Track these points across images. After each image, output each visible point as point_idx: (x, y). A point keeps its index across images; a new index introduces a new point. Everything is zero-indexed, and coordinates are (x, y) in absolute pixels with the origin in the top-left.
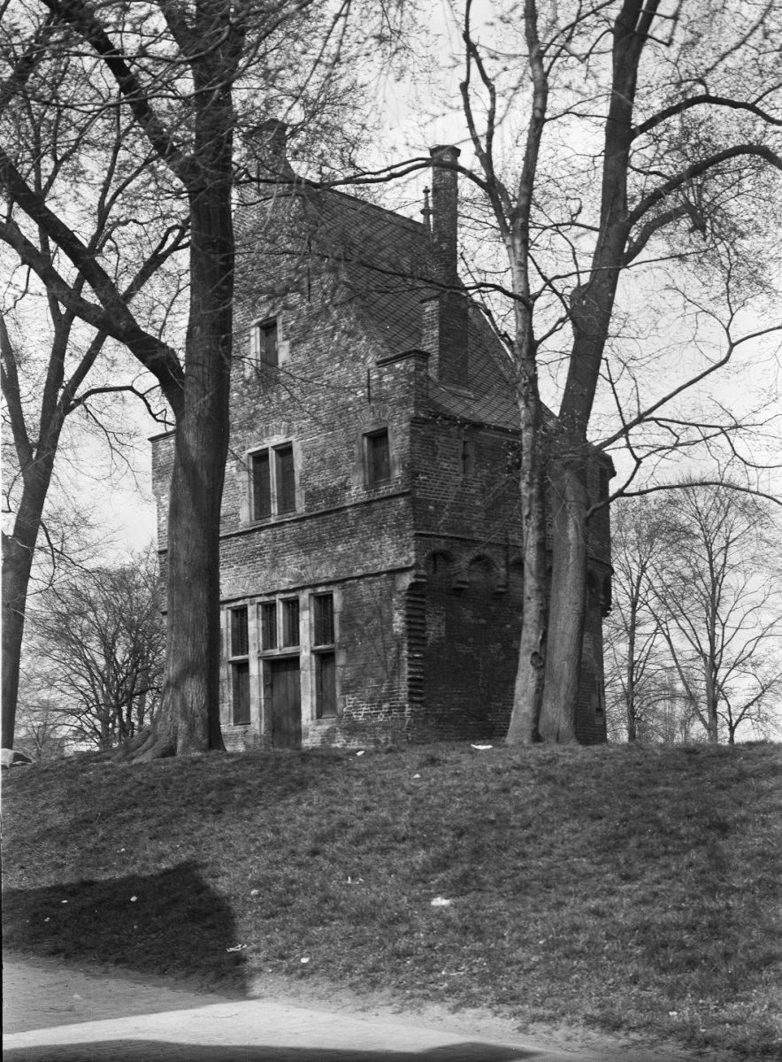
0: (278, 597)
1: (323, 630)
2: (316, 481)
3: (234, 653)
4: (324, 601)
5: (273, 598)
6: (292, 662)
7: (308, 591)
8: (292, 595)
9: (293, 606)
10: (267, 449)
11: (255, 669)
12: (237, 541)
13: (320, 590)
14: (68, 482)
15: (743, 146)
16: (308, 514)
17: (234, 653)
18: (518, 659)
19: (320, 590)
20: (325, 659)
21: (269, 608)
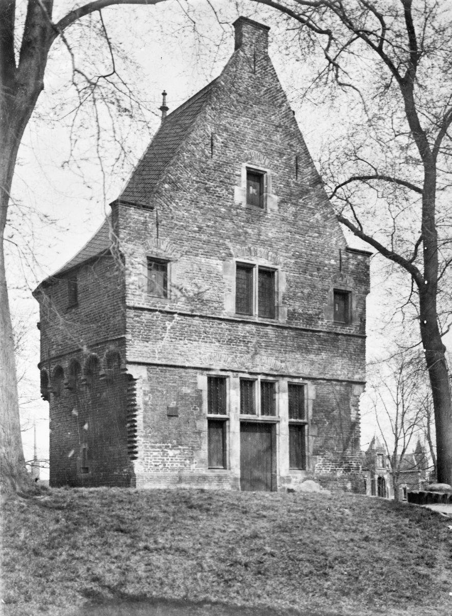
0: (260, 377)
1: (296, 408)
2: (297, 306)
3: (210, 411)
4: (296, 390)
5: (255, 377)
6: (269, 428)
7: (287, 379)
8: (271, 378)
9: (268, 387)
10: (254, 265)
11: (234, 427)
12: (220, 324)
13: (296, 381)
14: (445, 150)
15: (402, 258)
16: (287, 326)
17: (210, 411)
18: (50, 457)
19: (296, 381)
20: (297, 429)
21: (246, 384)
